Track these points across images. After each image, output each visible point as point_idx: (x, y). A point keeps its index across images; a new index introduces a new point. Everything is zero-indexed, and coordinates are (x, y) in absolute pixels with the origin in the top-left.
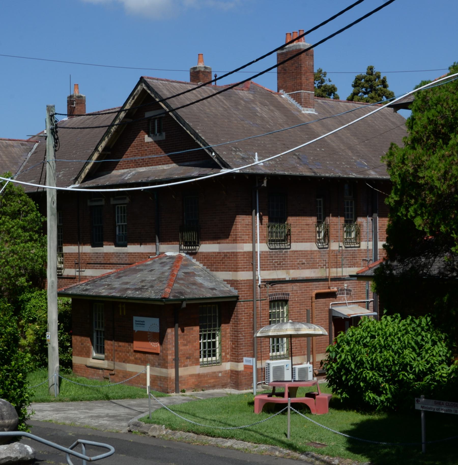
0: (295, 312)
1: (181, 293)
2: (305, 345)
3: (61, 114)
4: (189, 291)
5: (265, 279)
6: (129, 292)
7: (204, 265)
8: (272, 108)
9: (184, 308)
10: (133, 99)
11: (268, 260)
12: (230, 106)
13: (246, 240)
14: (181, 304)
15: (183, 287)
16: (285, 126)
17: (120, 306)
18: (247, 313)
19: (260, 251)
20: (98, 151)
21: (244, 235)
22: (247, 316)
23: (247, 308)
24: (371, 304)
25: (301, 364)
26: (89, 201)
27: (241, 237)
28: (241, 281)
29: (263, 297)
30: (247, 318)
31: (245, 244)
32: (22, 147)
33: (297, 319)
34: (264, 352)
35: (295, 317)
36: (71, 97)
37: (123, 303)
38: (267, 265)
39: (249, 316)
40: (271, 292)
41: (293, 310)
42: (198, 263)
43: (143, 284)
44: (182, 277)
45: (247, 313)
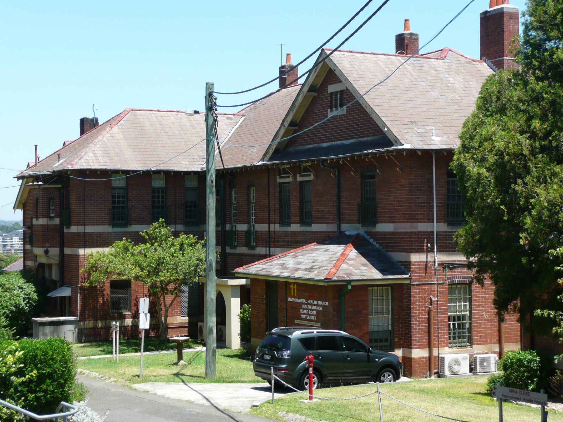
0: (479, 297)
1: (351, 274)
2: (425, 326)
3: (263, 85)
4: (356, 271)
5: (443, 261)
6: (299, 272)
7: (380, 246)
8: (468, 77)
9: (350, 290)
10: (315, 72)
11: (446, 240)
12: (417, 77)
13: (421, 219)
14: (346, 286)
15: (351, 268)
16: (130, 117)
17: (292, 286)
18: (422, 297)
19: (437, 232)
20: (284, 126)
21: (418, 214)
22: (422, 299)
23: (422, 292)
24: (82, 260)
25: (487, 353)
26: (278, 177)
27: (415, 216)
28: (415, 262)
29: (440, 281)
30: (422, 302)
31: (419, 224)
32: (227, 121)
33: (482, 305)
34: (441, 338)
35: (479, 302)
36: (283, 67)
37: (294, 283)
38: (446, 246)
39: (425, 300)
40: (449, 275)
41: (476, 295)
42: (375, 243)
43: (314, 264)
44: (354, 257)
45: (422, 297)
